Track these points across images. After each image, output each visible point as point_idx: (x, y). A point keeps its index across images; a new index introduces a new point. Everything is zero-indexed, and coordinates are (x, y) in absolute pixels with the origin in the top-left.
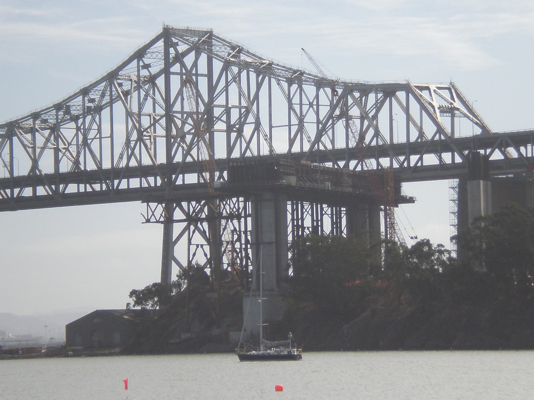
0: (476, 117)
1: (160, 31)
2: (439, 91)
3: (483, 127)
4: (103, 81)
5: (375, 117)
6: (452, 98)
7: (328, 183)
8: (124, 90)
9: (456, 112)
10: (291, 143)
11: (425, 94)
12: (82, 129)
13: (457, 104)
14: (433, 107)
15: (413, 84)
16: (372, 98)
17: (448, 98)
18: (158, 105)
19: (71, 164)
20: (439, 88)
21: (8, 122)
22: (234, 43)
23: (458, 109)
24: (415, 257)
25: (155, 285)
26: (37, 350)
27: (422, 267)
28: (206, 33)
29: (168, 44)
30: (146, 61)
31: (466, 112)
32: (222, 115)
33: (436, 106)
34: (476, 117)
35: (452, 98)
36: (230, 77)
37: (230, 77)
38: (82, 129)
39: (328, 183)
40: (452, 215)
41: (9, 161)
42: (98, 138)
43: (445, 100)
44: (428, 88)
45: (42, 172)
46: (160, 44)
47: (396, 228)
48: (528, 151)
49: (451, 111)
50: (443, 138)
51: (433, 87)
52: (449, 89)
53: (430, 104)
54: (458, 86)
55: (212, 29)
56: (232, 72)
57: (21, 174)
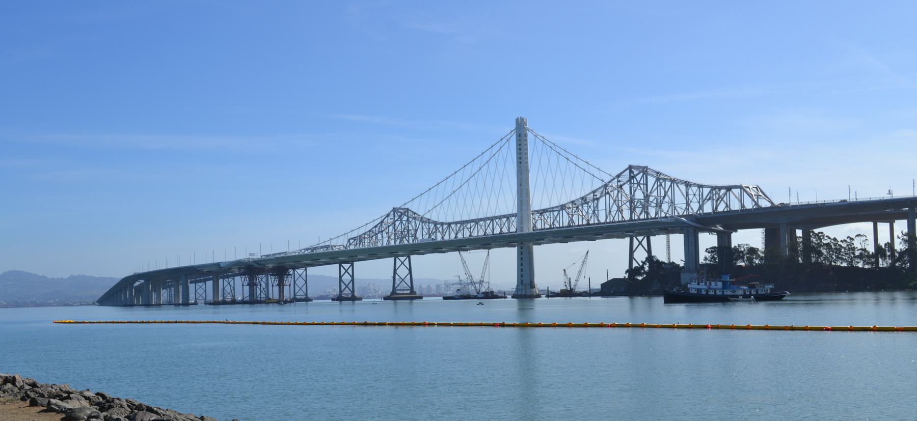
0: (768, 199)
1: (628, 167)
3: (772, 203)
6: (758, 190)
10: (606, 218)
11: (748, 189)
13: (761, 194)
15: (743, 186)
17: (756, 190)
19: (586, 222)
21: (818, 204)
22: (658, 171)
23: (761, 196)
25: (736, 231)
28: (645, 167)
29: (631, 172)
30: (620, 179)
32: (654, 200)
34: (768, 199)
35: (758, 190)
41: (893, 198)
44: (748, 187)
46: (628, 171)
51: (750, 187)
52: (756, 188)
54: (759, 186)
57: (720, 211)
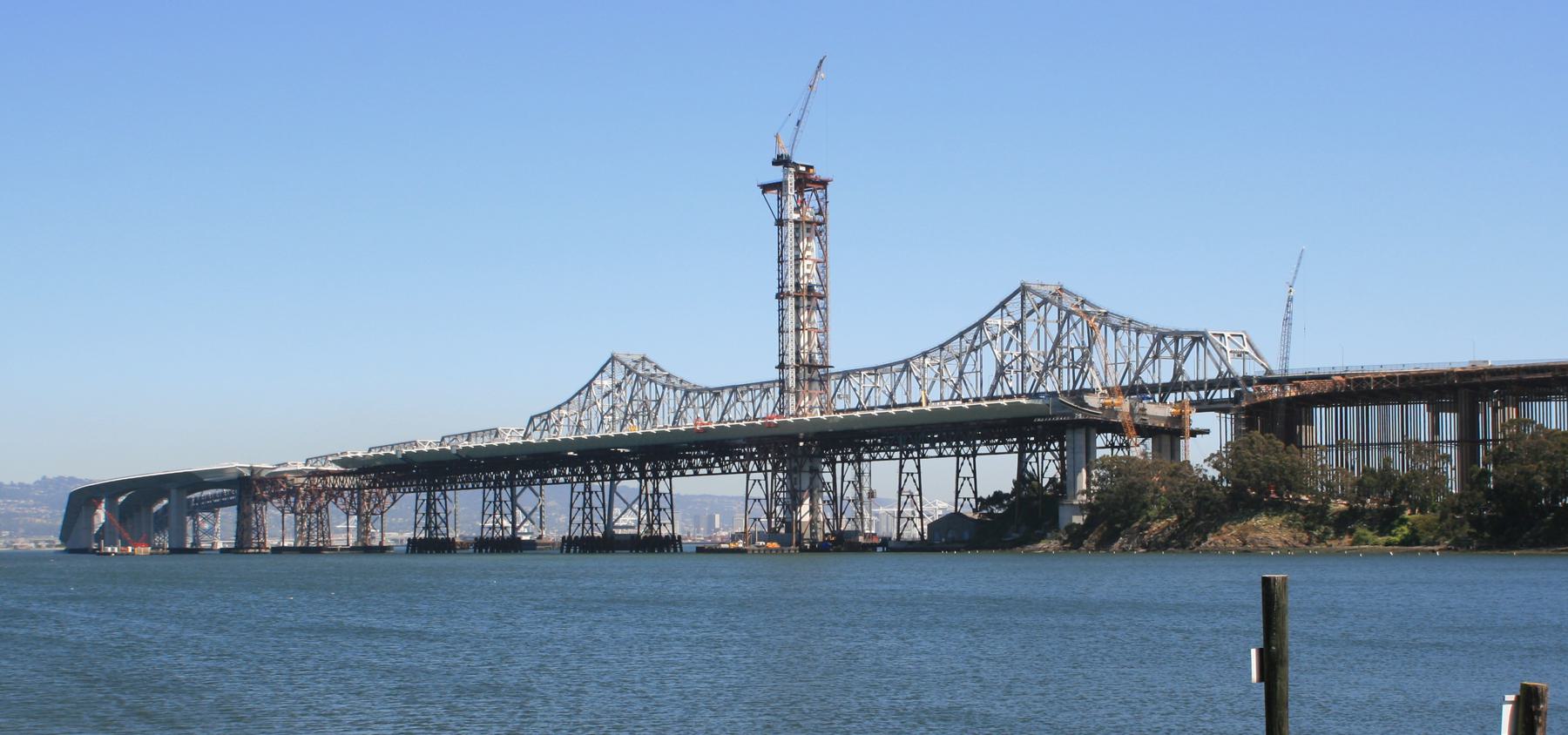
2: (1232, 338)
6: (1244, 345)
7: (870, 530)
9: (1246, 355)
12: (769, 471)
13: (1247, 348)
16: (1187, 341)
20: (1233, 335)
24: (1272, 486)
26: (1332, 501)
33: (1228, 350)
36: (1071, 325)
37: (1071, 325)
38: (769, 471)
39: (870, 530)
42: (1016, 452)
47: (997, 597)
48: (1552, 415)
50: (1232, 376)
51: (1227, 335)
55: (812, 167)
56: (1073, 320)
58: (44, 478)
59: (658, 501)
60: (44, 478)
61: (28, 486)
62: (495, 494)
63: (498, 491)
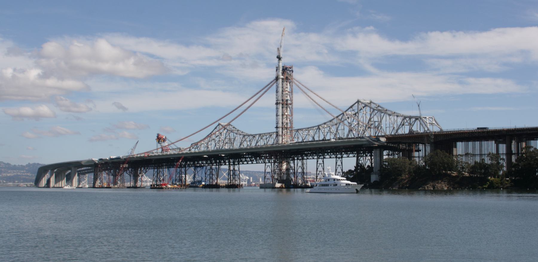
2: (429, 118)
4: (530, 131)
5: (233, 143)
6: (433, 121)
8: (515, 142)
9: (434, 124)
13: (434, 122)
14: (427, 123)
18: (135, 147)
20: (429, 118)
27: (432, 138)
31: (436, 124)
33: (428, 122)
35: (433, 121)
40: (515, 126)
43: (431, 121)
45: (454, 149)
49: (432, 124)
51: (427, 117)
53: (426, 122)
58: (29, 163)
59: (181, 170)
60: (29, 163)
61: (24, 166)
62: (210, 171)
63: (181, 168)
